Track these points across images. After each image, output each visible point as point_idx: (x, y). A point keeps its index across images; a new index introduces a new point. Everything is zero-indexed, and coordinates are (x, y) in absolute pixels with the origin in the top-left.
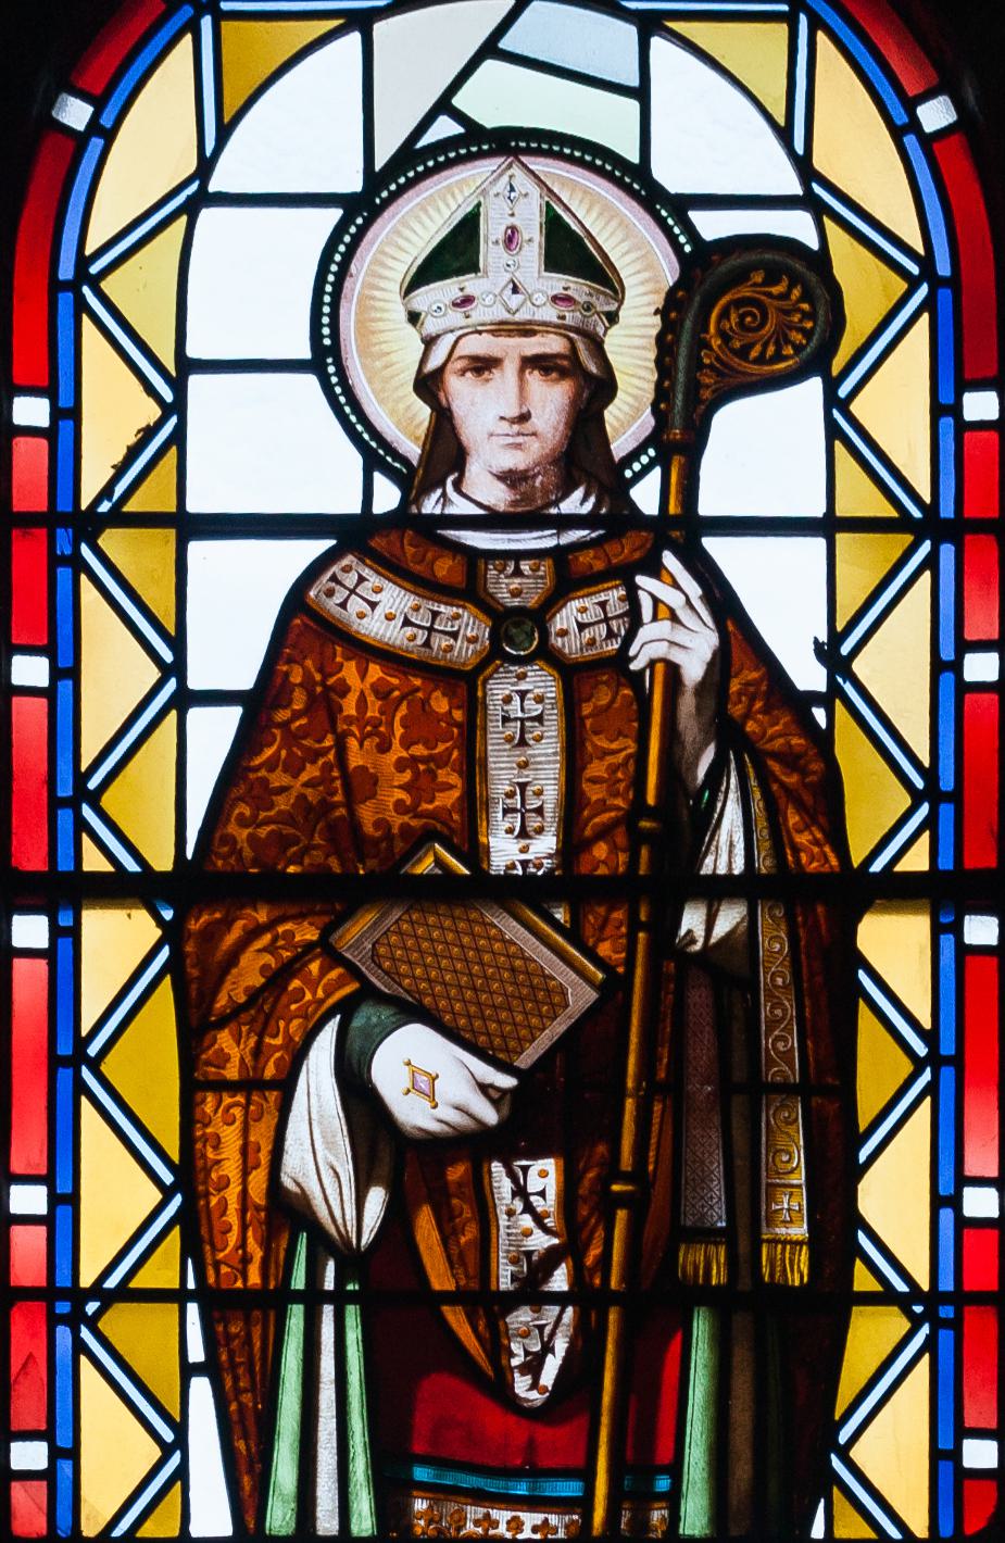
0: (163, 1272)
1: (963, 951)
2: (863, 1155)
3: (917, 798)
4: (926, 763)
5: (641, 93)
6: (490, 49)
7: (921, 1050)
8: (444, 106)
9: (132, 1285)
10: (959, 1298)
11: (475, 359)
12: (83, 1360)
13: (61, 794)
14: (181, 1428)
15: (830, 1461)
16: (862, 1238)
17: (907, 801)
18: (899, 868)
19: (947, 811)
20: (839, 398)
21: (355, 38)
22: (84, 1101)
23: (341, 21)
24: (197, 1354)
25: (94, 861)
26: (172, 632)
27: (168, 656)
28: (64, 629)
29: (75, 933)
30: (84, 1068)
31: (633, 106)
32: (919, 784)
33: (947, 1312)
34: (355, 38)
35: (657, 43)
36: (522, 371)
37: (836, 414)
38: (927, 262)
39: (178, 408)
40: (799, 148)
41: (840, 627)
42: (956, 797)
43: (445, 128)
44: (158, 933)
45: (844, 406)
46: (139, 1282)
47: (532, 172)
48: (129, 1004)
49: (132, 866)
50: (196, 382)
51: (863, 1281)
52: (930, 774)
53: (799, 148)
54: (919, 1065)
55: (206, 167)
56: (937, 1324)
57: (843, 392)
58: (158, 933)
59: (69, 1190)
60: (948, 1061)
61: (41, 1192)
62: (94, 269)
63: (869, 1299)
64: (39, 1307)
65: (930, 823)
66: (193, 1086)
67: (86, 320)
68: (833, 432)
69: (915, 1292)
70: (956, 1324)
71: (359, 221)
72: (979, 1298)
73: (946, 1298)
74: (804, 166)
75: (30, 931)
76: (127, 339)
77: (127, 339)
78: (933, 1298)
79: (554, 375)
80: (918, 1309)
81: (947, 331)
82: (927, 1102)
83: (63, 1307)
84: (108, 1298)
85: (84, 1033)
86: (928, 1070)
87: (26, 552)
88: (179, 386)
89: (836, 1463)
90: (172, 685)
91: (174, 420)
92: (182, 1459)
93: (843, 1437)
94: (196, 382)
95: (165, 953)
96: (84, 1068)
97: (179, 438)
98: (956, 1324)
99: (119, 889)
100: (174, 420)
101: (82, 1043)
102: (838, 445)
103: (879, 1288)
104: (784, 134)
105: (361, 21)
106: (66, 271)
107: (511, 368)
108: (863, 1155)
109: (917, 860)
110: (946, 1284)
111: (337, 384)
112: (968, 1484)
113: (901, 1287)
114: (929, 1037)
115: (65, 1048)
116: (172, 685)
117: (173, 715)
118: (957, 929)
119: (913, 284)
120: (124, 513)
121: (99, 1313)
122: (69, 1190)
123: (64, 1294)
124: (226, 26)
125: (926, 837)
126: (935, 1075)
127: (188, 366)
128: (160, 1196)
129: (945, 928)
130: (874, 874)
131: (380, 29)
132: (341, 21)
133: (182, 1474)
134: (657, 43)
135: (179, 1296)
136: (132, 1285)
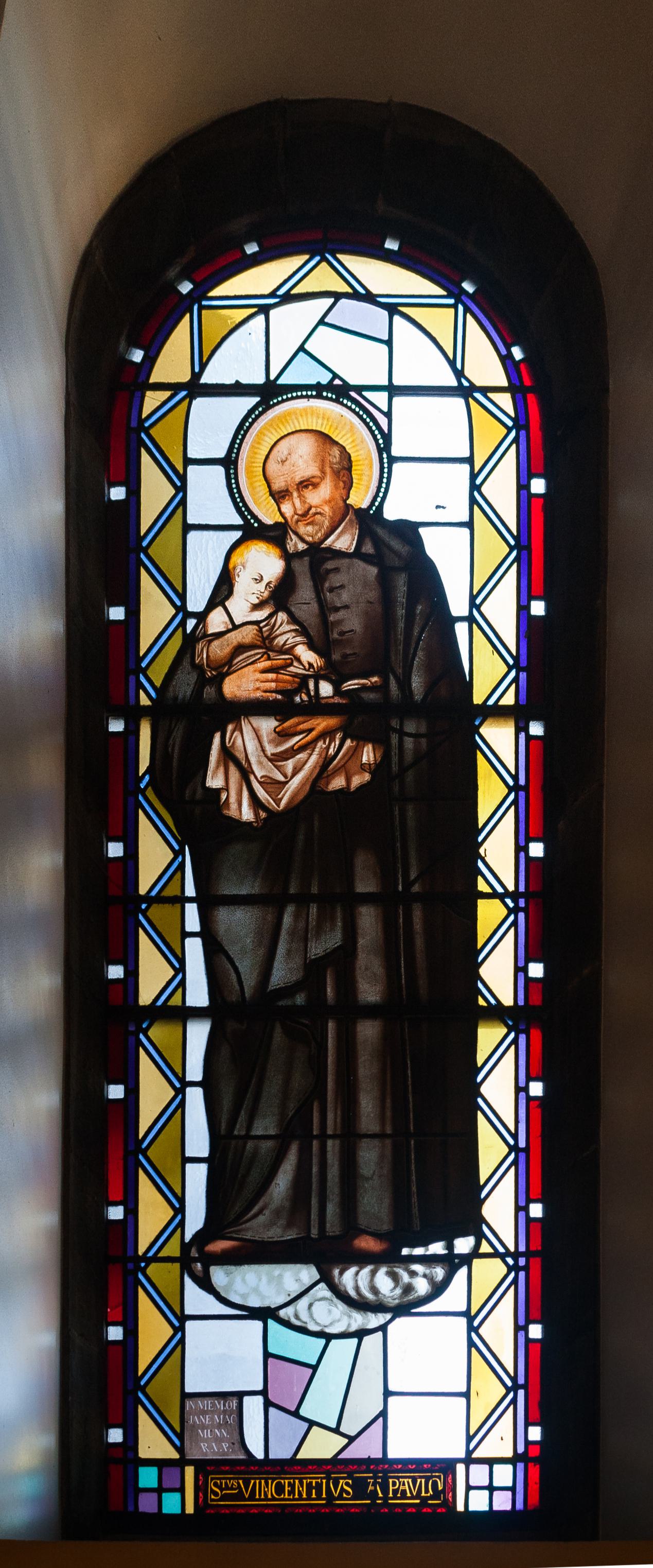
1: (529, 738)
2: (483, 1195)
3: (510, 789)
4: (512, 1374)
6: (322, 322)
7: (511, 783)
9: (159, 1255)
14: (182, 961)
17: (508, 550)
19: (522, 1156)
20: (474, 1326)
21: (261, 318)
27: (179, 603)
34: (261, 318)
37: (473, 1335)
39: (181, 488)
41: (475, 593)
42: (526, 788)
45: (477, 1330)
53: (459, 366)
54: (508, 1390)
57: (476, 1323)
60: (522, 1150)
68: (471, 1344)
69: (508, 1253)
71: (260, 409)
74: (459, 374)
75: (116, 726)
84: (149, 1261)
92: (183, 975)
97: (182, 1342)
100: (181, 495)
103: (491, 891)
104: (452, 363)
105: (265, 310)
108: (483, 1195)
109: (509, 699)
110: (522, 1248)
111: (254, 523)
115: (134, 424)
118: (526, 729)
119: (509, 430)
120: (179, 1332)
121: (147, 908)
125: (513, 1169)
129: (521, 728)
131: (273, 313)
134: (397, 319)
136: (159, 1255)
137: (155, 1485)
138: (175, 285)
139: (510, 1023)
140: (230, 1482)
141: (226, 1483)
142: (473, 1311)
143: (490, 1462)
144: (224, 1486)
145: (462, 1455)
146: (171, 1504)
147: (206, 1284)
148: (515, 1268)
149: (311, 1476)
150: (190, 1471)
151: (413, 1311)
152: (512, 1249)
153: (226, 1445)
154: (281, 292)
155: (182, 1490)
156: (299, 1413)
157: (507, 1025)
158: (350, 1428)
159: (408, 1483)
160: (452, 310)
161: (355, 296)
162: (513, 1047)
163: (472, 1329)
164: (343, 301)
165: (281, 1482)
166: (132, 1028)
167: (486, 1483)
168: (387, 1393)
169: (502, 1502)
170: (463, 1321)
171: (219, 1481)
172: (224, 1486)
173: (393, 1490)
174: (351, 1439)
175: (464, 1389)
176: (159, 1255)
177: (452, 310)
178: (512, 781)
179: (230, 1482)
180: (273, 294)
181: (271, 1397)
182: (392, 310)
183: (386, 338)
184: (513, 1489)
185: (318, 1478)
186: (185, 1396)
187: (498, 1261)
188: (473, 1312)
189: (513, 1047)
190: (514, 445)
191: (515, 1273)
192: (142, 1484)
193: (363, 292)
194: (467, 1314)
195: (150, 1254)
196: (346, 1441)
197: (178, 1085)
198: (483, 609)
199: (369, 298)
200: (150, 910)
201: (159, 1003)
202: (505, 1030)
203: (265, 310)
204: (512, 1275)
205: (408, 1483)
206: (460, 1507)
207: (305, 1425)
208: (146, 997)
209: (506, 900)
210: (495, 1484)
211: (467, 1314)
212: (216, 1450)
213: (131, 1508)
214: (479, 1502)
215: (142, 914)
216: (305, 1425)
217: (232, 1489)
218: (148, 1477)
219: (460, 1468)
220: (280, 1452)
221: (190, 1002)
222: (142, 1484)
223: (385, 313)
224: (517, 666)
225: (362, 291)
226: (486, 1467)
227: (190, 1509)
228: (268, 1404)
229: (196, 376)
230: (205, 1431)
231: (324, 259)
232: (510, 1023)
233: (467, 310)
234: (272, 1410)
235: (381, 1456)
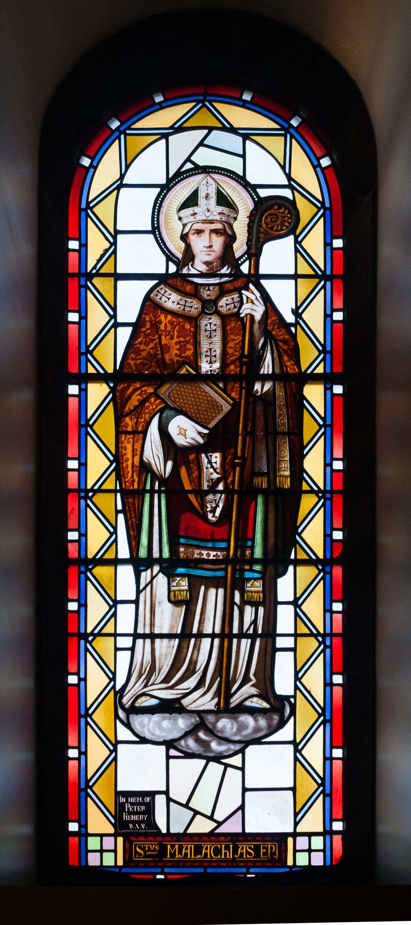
0: (110, 484)
3: (320, 352)
4: (323, 343)
5: (243, 156)
6: (201, 144)
7: (321, 422)
8: (188, 160)
9: (102, 488)
10: (332, 492)
11: (197, 230)
12: (88, 509)
13: (82, 351)
15: (296, 537)
16: (305, 475)
18: (315, 372)
19: (328, 356)
21: (164, 141)
22: (88, 437)
23: (160, 136)
24: (120, 507)
25: (91, 370)
26: (113, 306)
28: (83, 305)
29: (86, 390)
30: (88, 428)
31: (241, 160)
32: (321, 348)
33: (328, 496)
34: (164, 141)
35: (248, 142)
36: (210, 233)
37: (298, 755)
38: (323, 203)
39: (115, 750)
40: (287, 171)
41: (299, 305)
42: (331, 352)
43: (189, 166)
44: (109, 390)
45: (300, 752)
46: (105, 631)
47: (213, 178)
48: (101, 410)
49: (102, 371)
50: (120, 746)
51: (305, 487)
52: (324, 346)
53: (287, 171)
54: (321, 427)
55: (122, 176)
56: (325, 209)
57: (299, 239)
58: (109, 390)
59: (84, 462)
60: (329, 426)
61: (76, 462)
62: (91, 205)
63: (307, 492)
64: (76, 494)
65: (324, 360)
66: (119, 432)
67: (88, 437)
68: (296, 759)
70: (331, 499)
72: (337, 492)
73: (328, 492)
74: (289, 176)
75: (73, 389)
76: (100, 224)
77: (100, 224)
78: (325, 492)
79: (219, 235)
80: (320, 495)
81: (328, 222)
82: (323, 437)
83: (83, 494)
85: (88, 418)
86: (323, 428)
87: (72, 284)
88: (115, 746)
89: (298, 538)
90: (113, 321)
91: (113, 247)
93: (299, 531)
94: (119, 237)
95: (111, 396)
96: (88, 428)
98: (331, 499)
99: (98, 378)
100: (113, 247)
101: (88, 421)
102: (298, 618)
103: (309, 489)
104: (283, 167)
105: (166, 136)
106: (83, 206)
107: (207, 232)
108: (305, 452)
109: (320, 370)
112: (334, 544)
113: (315, 632)
114: (324, 419)
116: (113, 321)
117: (113, 329)
121: (93, 496)
122: (84, 462)
123: (83, 491)
124: (128, 137)
125: (322, 363)
126: (325, 430)
127: (118, 742)
128: (109, 463)
129: (328, 389)
130: (308, 373)
131: (171, 138)
132: (160, 136)
133: (116, 541)
134: (248, 142)
135: (115, 491)
136: (102, 488)
137: (98, 848)
138: (108, 123)
139: (320, 567)
140: (152, 846)
141: (149, 848)
142: (298, 740)
143: (310, 835)
144: (147, 849)
145: (291, 830)
146: (109, 860)
147: (128, 725)
148: (324, 497)
149: (186, 843)
150: (120, 840)
151: (233, 691)
152: (322, 631)
153: (143, 825)
154: (176, 126)
155: (115, 851)
156: (293, 838)
157: (318, 568)
158: (219, 816)
159: (191, 848)
160: (283, 138)
161: (224, 129)
162: (322, 654)
163: (297, 750)
164: (214, 132)
165: (218, 847)
166: (83, 569)
167: (307, 847)
168: (245, 790)
169: (318, 860)
170: (291, 747)
171: (219, 846)
172: (147, 849)
173: (263, 852)
174: (220, 824)
175: (292, 785)
176: (104, 558)
177: (283, 138)
178: (321, 421)
179: (152, 846)
180: (172, 127)
181: (172, 795)
182: (246, 137)
183: (241, 153)
184: (324, 851)
185: (211, 844)
186: (118, 794)
187: (313, 639)
188: (298, 741)
189: (322, 654)
190: (322, 218)
191: (324, 282)
192: (90, 848)
193: (228, 126)
194: (294, 743)
195: (96, 488)
196: (216, 825)
197: (111, 603)
198: (303, 244)
199: (233, 130)
200: (94, 497)
201: (98, 557)
202: (317, 499)
203: (166, 136)
204: (322, 355)
205: (191, 848)
206: (290, 862)
207: (192, 813)
208: (92, 549)
209: (317, 489)
210: (104, 854)
211: (294, 743)
212: (138, 828)
213: (83, 864)
214: (302, 860)
215: (89, 500)
216: (192, 813)
217: (154, 851)
218: (93, 843)
219: (290, 840)
220: (177, 828)
221: (120, 556)
222: (90, 848)
223: (240, 139)
224: (324, 351)
225: (228, 126)
226: (307, 838)
227: (120, 863)
228: (169, 800)
229: (122, 176)
230: (132, 798)
231: (204, 106)
232: (320, 567)
233: (292, 137)
234: (171, 804)
235: (241, 831)
